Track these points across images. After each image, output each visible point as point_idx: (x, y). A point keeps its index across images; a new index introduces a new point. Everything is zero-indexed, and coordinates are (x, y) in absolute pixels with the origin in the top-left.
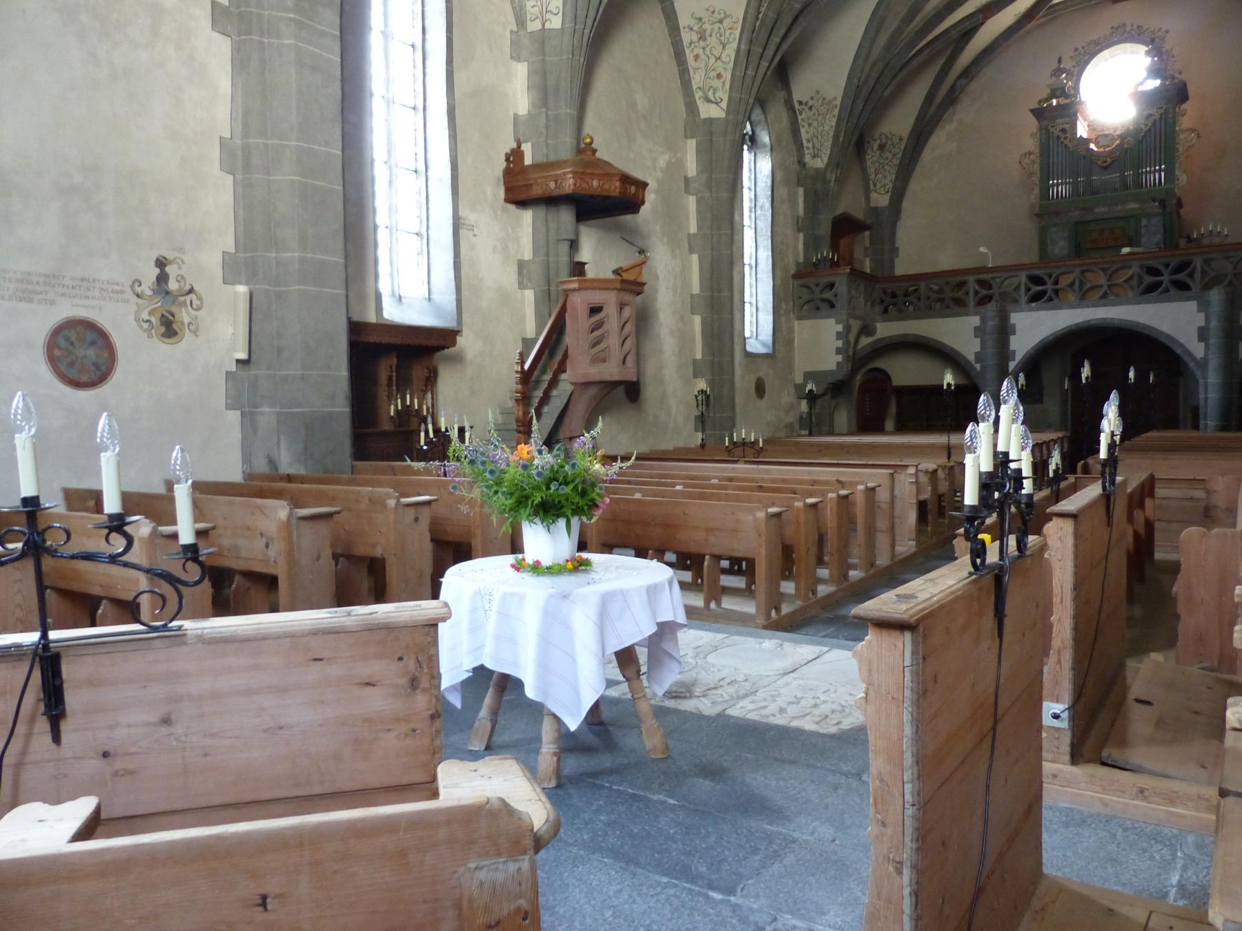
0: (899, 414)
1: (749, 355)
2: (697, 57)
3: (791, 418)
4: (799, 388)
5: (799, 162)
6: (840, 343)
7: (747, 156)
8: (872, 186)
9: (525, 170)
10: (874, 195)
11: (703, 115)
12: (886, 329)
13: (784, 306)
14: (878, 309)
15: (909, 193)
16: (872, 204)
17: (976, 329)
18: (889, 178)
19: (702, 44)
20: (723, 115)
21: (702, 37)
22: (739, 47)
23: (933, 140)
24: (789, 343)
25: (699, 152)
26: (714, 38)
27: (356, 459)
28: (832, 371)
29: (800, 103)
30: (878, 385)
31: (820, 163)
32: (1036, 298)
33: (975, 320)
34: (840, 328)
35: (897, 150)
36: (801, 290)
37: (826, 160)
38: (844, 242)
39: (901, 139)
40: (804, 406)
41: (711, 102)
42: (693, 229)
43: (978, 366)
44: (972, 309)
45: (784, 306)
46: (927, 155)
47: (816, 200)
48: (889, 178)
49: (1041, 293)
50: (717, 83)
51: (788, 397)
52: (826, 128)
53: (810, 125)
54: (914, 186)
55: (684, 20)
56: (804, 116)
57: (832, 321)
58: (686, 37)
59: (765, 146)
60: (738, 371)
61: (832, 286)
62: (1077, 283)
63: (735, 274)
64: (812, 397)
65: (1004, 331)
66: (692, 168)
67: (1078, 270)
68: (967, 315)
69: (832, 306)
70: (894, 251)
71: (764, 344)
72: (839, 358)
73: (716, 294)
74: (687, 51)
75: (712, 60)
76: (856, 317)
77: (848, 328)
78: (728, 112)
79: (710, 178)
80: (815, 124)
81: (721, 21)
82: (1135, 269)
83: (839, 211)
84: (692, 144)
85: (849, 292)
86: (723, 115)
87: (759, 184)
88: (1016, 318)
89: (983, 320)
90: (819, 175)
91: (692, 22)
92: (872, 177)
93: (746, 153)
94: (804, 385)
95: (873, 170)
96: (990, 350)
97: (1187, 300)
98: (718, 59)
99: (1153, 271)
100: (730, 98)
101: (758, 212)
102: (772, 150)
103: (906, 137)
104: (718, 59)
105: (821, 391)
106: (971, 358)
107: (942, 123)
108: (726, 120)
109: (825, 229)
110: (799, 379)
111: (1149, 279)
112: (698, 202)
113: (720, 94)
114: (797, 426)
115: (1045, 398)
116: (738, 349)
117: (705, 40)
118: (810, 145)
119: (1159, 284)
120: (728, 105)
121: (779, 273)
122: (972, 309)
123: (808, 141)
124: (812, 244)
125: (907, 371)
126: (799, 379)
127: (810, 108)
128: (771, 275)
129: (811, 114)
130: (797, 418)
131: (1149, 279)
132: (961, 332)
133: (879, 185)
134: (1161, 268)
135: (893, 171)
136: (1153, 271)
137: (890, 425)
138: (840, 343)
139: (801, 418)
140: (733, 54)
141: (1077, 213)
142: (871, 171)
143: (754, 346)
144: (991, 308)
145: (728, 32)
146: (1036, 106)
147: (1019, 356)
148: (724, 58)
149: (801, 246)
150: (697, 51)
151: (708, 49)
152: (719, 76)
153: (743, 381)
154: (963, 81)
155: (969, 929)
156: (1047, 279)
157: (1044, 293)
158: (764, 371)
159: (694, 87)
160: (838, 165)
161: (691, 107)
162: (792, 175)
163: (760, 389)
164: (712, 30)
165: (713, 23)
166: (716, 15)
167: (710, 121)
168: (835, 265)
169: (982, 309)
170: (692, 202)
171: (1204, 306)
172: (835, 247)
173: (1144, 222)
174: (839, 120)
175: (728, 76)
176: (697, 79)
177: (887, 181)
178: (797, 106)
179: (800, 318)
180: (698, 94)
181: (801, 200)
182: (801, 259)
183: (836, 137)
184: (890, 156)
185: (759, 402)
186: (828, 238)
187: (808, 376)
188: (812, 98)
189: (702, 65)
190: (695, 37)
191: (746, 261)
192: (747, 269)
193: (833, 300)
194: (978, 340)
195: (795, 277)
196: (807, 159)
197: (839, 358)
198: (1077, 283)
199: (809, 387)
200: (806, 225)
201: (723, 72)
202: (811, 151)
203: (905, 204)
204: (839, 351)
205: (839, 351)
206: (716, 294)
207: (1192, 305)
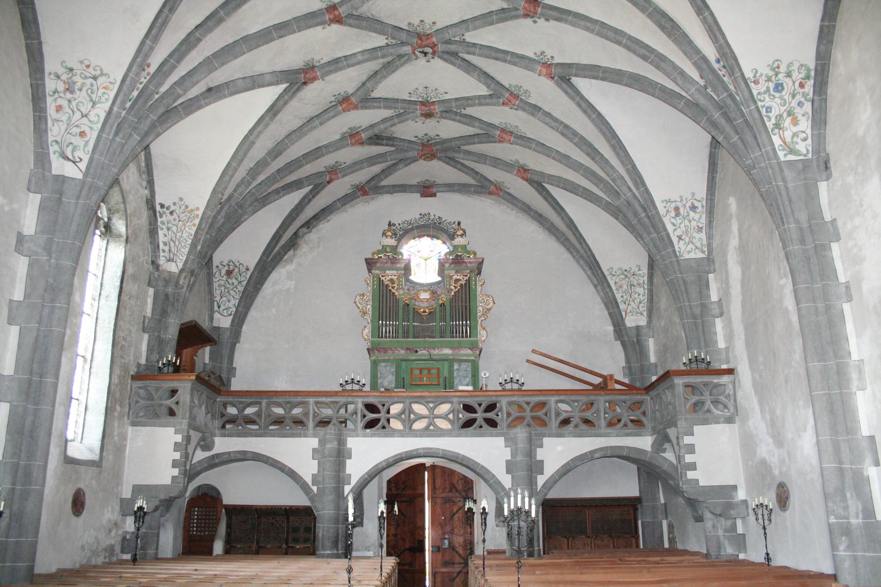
0: (228, 534)
1: (70, 461)
2: (59, 108)
3: (114, 539)
4: (125, 506)
5: (153, 262)
6: (177, 456)
7: (98, 243)
8: (216, 308)
10: (216, 316)
11: (55, 171)
12: (223, 444)
13: (118, 408)
14: (217, 423)
15: (249, 318)
16: (215, 325)
17: (314, 450)
18: (233, 302)
19: (69, 96)
20: (80, 176)
21: (70, 89)
22: (111, 109)
23: (274, 276)
24: (120, 450)
25: (42, 208)
26: (84, 93)
28: (165, 486)
29: (162, 206)
30: (206, 501)
31: (174, 268)
32: (371, 424)
33: (314, 442)
34: (179, 438)
35: (243, 279)
36: (139, 392)
37: (180, 265)
38: (187, 352)
39: (247, 269)
40: (130, 524)
41: (69, 159)
42: (18, 295)
43: (315, 489)
44: (311, 431)
45: (118, 408)
46: (268, 288)
47: (165, 304)
48: (233, 302)
49: (374, 420)
50: (78, 141)
51: (111, 513)
52: (185, 235)
53: (168, 229)
54: (253, 313)
55: (51, 65)
56: (164, 219)
57: (171, 430)
58: (50, 84)
59: (120, 236)
60: (51, 481)
61: (174, 392)
63: (64, 360)
64: (140, 515)
65: (341, 455)
66: (29, 224)
68: (306, 436)
69: (172, 413)
70: (232, 371)
71: (91, 450)
72: (176, 472)
73: (36, 378)
74: (49, 100)
75: (78, 115)
76: (196, 429)
77: (188, 439)
78: (86, 174)
79: (50, 242)
80: (174, 229)
81: (95, 78)
83: (186, 319)
84: (35, 200)
85: (192, 401)
86: (80, 176)
87: (106, 272)
88: (353, 443)
89: (322, 442)
90: (170, 279)
91: (61, 70)
92: (218, 299)
93: (97, 238)
94: (133, 500)
95: (218, 292)
96: (329, 473)
97: (497, 435)
98: (84, 116)
99: (468, 408)
100: (91, 160)
101: (103, 301)
102: (127, 241)
103: (252, 268)
104: (84, 116)
105: (152, 508)
106: (309, 480)
107: (282, 263)
108: (83, 182)
109: (172, 333)
110: (127, 494)
112: (31, 265)
113: (79, 154)
114: (118, 549)
115: (365, 521)
116: (54, 453)
117: (72, 92)
118: (167, 248)
119: (523, 418)
120: (88, 168)
121: (117, 372)
122: (311, 431)
123: (165, 244)
124: (156, 346)
125: (241, 489)
126: (127, 494)
127: (172, 213)
129: (171, 218)
130: (120, 539)
133: (222, 307)
134: (476, 407)
135: (238, 297)
136: (468, 408)
137: (218, 547)
138: (177, 456)
139: (124, 539)
140: (103, 116)
141: (402, 352)
142: (217, 293)
143: (75, 451)
144: (331, 429)
145: (101, 91)
146: (370, 256)
148: (92, 116)
149: (144, 347)
150: (60, 102)
151: (74, 103)
152: (82, 134)
153: (54, 489)
154: (305, 230)
156: (380, 407)
158: (87, 481)
159: (50, 139)
160: (192, 273)
161: (42, 159)
162: (143, 271)
163: (78, 504)
164: (83, 84)
165: (86, 78)
166: (91, 70)
167: (62, 180)
168: (177, 369)
169: (321, 431)
170: (21, 265)
171: (510, 442)
172: (178, 354)
173: (456, 366)
174: (199, 228)
175: (92, 136)
176: (55, 132)
177: (231, 305)
178: (158, 208)
179: (134, 424)
180: (53, 148)
181: (150, 301)
182: (143, 361)
183: (193, 245)
184: (236, 283)
185: (74, 518)
186: (174, 344)
187: (138, 490)
188: (174, 204)
189: (65, 118)
190: (61, 87)
191: (81, 350)
192: (80, 361)
193: (174, 407)
194: (538, 458)
195: (134, 378)
196: (162, 261)
197: (176, 472)
199: (139, 503)
200: (154, 326)
201: (88, 131)
202: (166, 254)
203: (245, 328)
204: (175, 464)
205: (175, 464)
206: (36, 378)
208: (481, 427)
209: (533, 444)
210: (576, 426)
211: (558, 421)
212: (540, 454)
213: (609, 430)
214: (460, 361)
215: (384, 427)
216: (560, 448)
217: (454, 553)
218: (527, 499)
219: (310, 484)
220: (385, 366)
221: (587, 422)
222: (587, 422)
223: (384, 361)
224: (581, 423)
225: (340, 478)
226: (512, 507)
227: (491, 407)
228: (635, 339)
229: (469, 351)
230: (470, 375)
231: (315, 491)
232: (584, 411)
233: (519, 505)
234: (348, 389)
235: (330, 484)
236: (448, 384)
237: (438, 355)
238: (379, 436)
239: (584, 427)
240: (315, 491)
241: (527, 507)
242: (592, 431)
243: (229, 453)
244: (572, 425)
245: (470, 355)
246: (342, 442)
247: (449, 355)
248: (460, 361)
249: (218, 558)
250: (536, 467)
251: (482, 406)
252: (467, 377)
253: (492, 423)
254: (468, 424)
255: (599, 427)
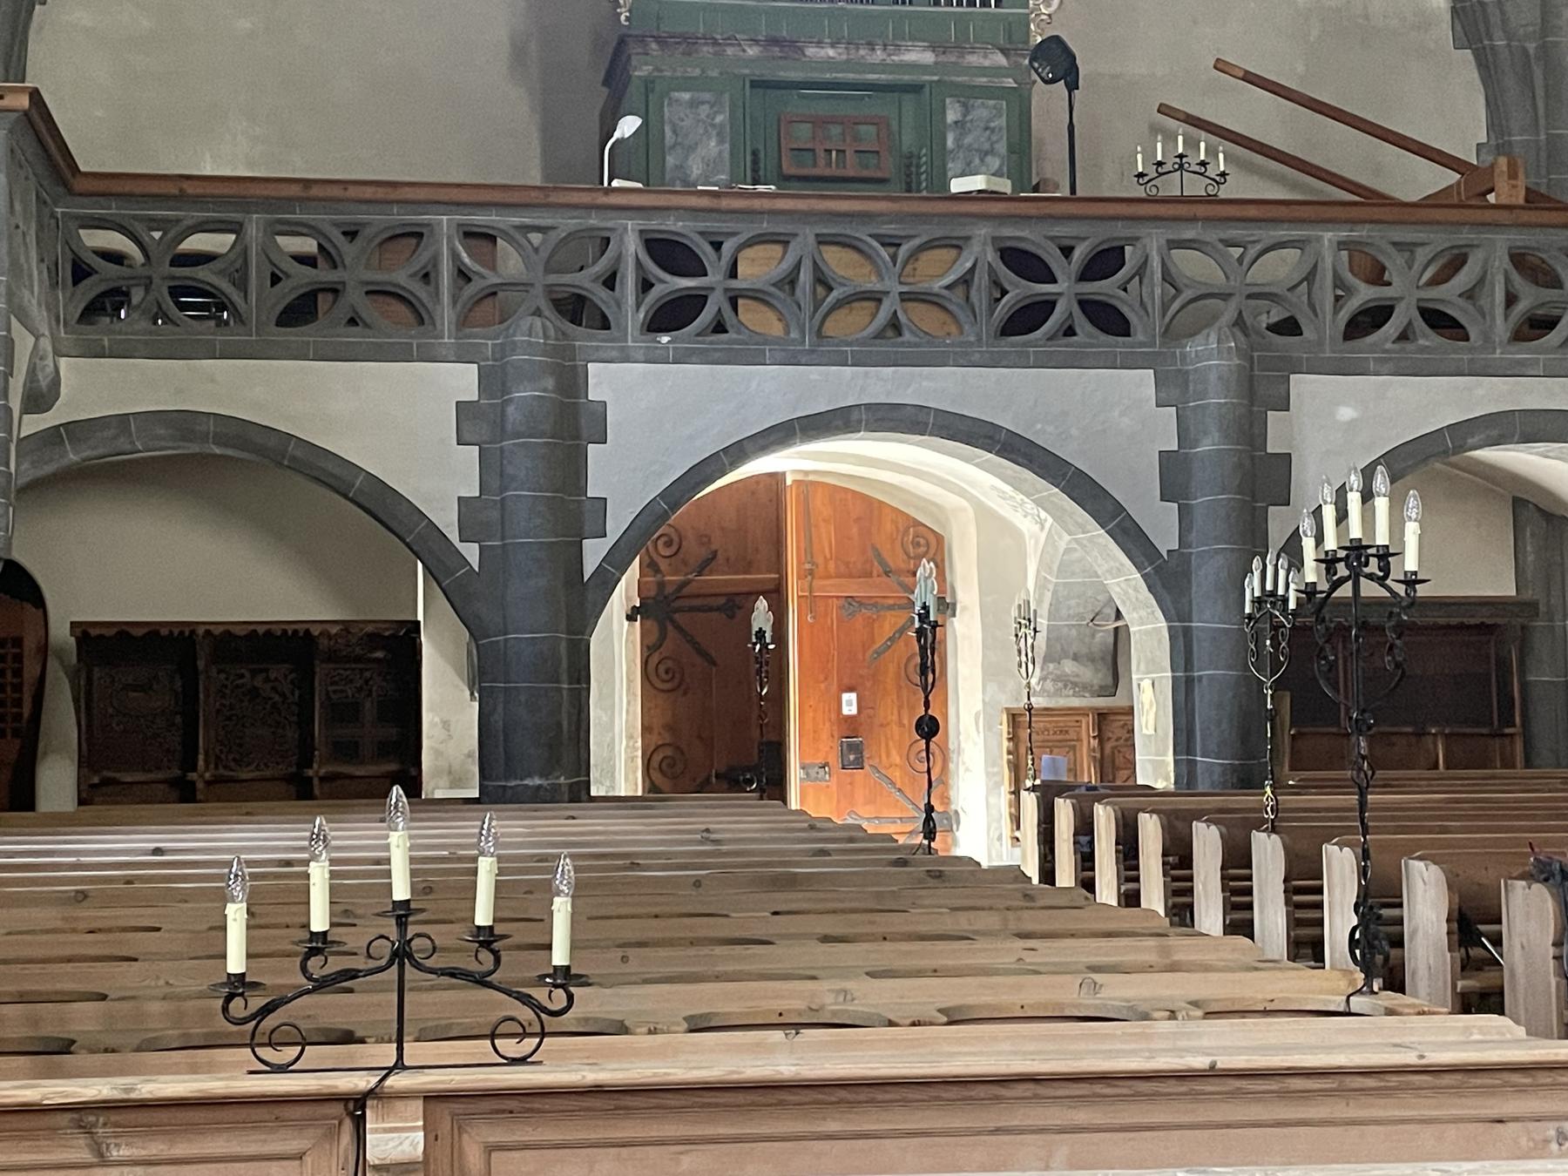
9: (395, 779)
27: (1292, 318)
32: (672, 316)
43: (471, 552)
62: (805, 277)
65: (574, 425)
67: (808, 234)
82: (980, 251)
99: (1023, 262)
106: (447, 520)
111: (1020, 290)
128: (45, 704)
131: (1020, 290)
132: (403, 419)
137: (57, 780)
141: (752, 51)
147: (617, 523)
155: (5, 962)
156: (705, 250)
157: (696, 302)
198: (805, 277)
207: (1142, 381)
208: (1070, 332)
209: (1261, 393)
210: (1404, 337)
211: (1342, 325)
212: (1278, 433)
213: (1522, 353)
214: (967, 94)
215: (720, 328)
216: (1346, 413)
217: (348, 1125)
218: (1282, 573)
219: (454, 536)
220: (694, 104)
221: (1438, 320)
222: (1438, 320)
223: (687, 84)
224: (1419, 323)
225: (575, 513)
226: (1331, 543)
227: (1105, 262)
228: (1531, 47)
229: (1000, 60)
230: (1002, 147)
231: (474, 560)
232: (1436, 281)
233: (1356, 532)
234: (481, 211)
235: (530, 534)
236: (919, 175)
237: (883, 67)
238: (705, 358)
239: (1428, 339)
240: (474, 560)
241: (1281, 592)
242: (1457, 352)
243: (122, 421)
244: (1391, 328)
245: (996, 71)
246: (572, 382)
247: (924, 68)
248: (967, 94)
249: (59, 823)
250: (1264, 480)
251: (1077, 254)
252: (991, 152)
253: (1109, 319)
254: (1026, 319)
255: (1487, 337)
